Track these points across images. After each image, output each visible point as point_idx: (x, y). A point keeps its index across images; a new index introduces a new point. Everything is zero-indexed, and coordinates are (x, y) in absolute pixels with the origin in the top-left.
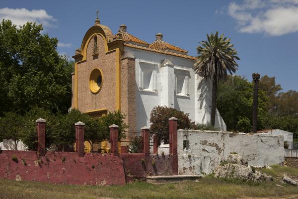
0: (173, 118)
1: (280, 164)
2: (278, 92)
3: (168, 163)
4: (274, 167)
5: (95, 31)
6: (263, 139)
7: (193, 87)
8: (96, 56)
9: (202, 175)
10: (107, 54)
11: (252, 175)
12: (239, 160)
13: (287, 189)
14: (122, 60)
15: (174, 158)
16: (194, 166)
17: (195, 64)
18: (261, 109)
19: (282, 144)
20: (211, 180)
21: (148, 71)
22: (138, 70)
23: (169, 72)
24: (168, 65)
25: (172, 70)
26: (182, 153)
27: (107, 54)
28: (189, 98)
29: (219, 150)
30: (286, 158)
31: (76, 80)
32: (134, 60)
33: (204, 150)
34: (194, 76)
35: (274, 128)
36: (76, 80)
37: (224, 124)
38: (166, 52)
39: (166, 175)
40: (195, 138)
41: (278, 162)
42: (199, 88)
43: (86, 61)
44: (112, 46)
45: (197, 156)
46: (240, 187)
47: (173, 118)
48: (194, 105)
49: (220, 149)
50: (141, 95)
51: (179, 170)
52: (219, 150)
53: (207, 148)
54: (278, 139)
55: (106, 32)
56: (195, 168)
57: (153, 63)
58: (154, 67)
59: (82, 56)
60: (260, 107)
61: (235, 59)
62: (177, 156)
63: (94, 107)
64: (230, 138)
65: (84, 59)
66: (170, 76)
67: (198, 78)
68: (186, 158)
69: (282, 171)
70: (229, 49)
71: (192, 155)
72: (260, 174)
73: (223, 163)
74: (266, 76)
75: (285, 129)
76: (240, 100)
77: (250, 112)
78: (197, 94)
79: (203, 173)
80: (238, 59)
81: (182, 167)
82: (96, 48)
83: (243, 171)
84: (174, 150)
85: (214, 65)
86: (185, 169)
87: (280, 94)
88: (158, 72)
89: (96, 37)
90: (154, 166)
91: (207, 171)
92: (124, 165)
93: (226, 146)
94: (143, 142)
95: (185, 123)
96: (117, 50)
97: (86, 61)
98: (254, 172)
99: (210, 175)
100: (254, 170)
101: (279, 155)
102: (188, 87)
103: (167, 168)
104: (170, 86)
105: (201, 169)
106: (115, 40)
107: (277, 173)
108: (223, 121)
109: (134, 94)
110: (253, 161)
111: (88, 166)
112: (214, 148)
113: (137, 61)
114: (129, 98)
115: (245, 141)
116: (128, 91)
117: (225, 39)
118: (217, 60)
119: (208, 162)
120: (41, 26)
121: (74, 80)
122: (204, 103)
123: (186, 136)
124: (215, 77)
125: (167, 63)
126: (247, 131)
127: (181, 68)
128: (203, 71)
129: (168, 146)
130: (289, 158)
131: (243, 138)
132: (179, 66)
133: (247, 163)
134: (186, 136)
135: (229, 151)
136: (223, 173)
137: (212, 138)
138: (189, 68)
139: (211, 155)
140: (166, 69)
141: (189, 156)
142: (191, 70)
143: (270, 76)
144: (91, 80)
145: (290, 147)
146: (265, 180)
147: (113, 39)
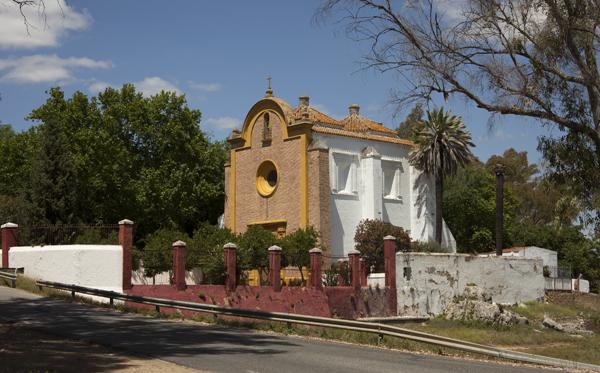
0: (389, 237)
1: (538, 300)
2: (533, 177)
3: (384, 300)
4: (530, 304)
5: (265, 108)
6: (513, 263)
7: (408, 185)
8: (267, 143)
9: (429, 316)
10: (285, 141)
12: (479, 295)
13: (549, 336)
14: (310, 151)
15: (391, 292)
17: (410, 154)
18: (508, 216)
19: (541, 270)
20: (441, 323)
21: (345, 163)
22: (332, 163)
23: (374, 165)
24: (373, 157)
25: (379, 162)
26: (402, 285)
27: (285, 141)
28: (401, 202)
29: (452, 280)
30: (547, 292)
31: (233, 175)
32: (327, 151)
33: (431, 281)
34: (408, 169)
35: (528, 244)
36: (233, 175)
37: (452, 238)
38: (369, 135)
39: (383, 316)
40: (420, 263)
41: (535, 297)
42: (415, 187)
43: (250, 148)
44: (294, 131)
46: (484, 332)
47: (389, 237)
48: (408, 212)
52: (452, 280)
53: (435, 277)
54: (535, 263)
55: (284, 109)
57: (350, 153)
58: (353, 159)
59: (245, 141)
60: (507, 212)
61: (468, 146)
62: (396, 291)
63: (264, 216)
64: (466, 264)
65: (246, 145)
66: (376, 171)
67: (414, 172)
68: (408, 293)
69: (541, 310)
70: (459, 132)
72: (510, 314)
73: (457, 299)
74: (512, 150)
75: (544, 246)
76: (476, 202)
77: (492, 220)
78: (413, 195)
79: (430, 314)
80: (473, 145)
82: (267, 131)
83: (487, 310)
84: (391, 281)
85: (438, 155)
86: (406, 307)
87: (536, 179)
88: (358, 165)
89: (267, 114)
90: (366, 304)
91: (436, 311)
92: (329, 302)
93: (460, 275)
94: (351, 271)
95: (404, 242)
96: (303, 136)
97: (250, 148)
98: (502, 312)
99: (440, 316)
100: (501, 308)
101: (536, 287)
102: (400, 185)
103: (382, 306)
104: (375, 186)
105: (428, 307)
106: (298, 123)
107: (533, 313)
108: (451, 236)
109: (327, 199)
111: (287, 304)
112: (445, 278)
113: (331, 151)
114: (321, 206)
115: (487, 267)
116: (321, 196)
117: (454, 117)
118: (442, 148)
119: (436, 298)
120: (183, 97)
121: (230, 174)
122: (424, 209)
123: (407, 261)
124: (440, 171)
125: (372, 154)
126: (488, 251)
128: (422, 163)
129: (383, 275)
130: (551, 290)
131: (486, 261)
133: (491, 299)
134: (407, 261)
136: (458, 313)
137: (441, 263)
138: (401, 157)
139: (441, 287)
140: (370, 161)
141: (412, 290)
142: (404, 161)
143: (518, 150)
144: (258, 176)
145: (552, 275)
146: (517, 323)
147: (296, 120)
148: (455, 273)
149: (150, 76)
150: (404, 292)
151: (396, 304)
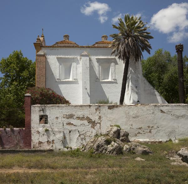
9: (66, 150)
11: (102, 146)
16: (53, 141)
21: (66, 64)
29: (93, 124)
33: (69, 124)
45: (58, 130)
49: (94, 122)
50: (59, 85)
51: (32, 144)
52: (93, 124)
56: (55, 142)
62: (30, 131)
64: (109, 110)
71: (50, 129)
81: (38, 141)
93: (104, 118)
110: (149, 134)
112: (86, 122)
119: (75, 136)
127: (105, 57)
132: (103, 55)
135: (109, 124)
139: (81, 129)
141: (47, 131)
148: (97, 118)
149: (166, 6)
150: (38, 132)
151: (30, 140)
